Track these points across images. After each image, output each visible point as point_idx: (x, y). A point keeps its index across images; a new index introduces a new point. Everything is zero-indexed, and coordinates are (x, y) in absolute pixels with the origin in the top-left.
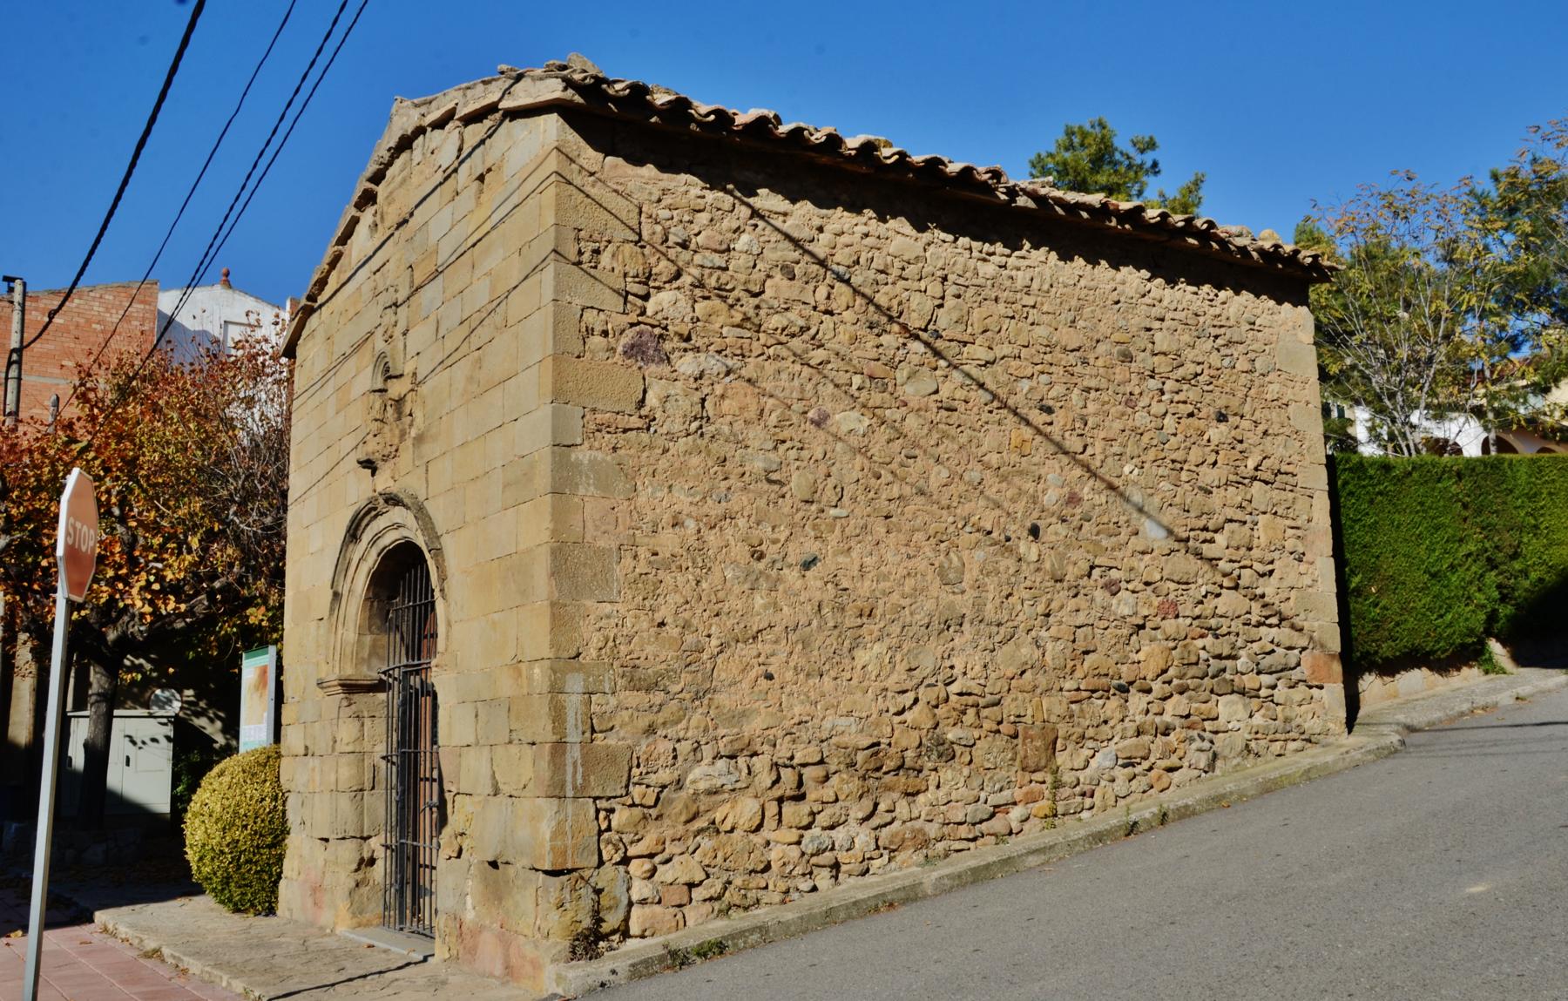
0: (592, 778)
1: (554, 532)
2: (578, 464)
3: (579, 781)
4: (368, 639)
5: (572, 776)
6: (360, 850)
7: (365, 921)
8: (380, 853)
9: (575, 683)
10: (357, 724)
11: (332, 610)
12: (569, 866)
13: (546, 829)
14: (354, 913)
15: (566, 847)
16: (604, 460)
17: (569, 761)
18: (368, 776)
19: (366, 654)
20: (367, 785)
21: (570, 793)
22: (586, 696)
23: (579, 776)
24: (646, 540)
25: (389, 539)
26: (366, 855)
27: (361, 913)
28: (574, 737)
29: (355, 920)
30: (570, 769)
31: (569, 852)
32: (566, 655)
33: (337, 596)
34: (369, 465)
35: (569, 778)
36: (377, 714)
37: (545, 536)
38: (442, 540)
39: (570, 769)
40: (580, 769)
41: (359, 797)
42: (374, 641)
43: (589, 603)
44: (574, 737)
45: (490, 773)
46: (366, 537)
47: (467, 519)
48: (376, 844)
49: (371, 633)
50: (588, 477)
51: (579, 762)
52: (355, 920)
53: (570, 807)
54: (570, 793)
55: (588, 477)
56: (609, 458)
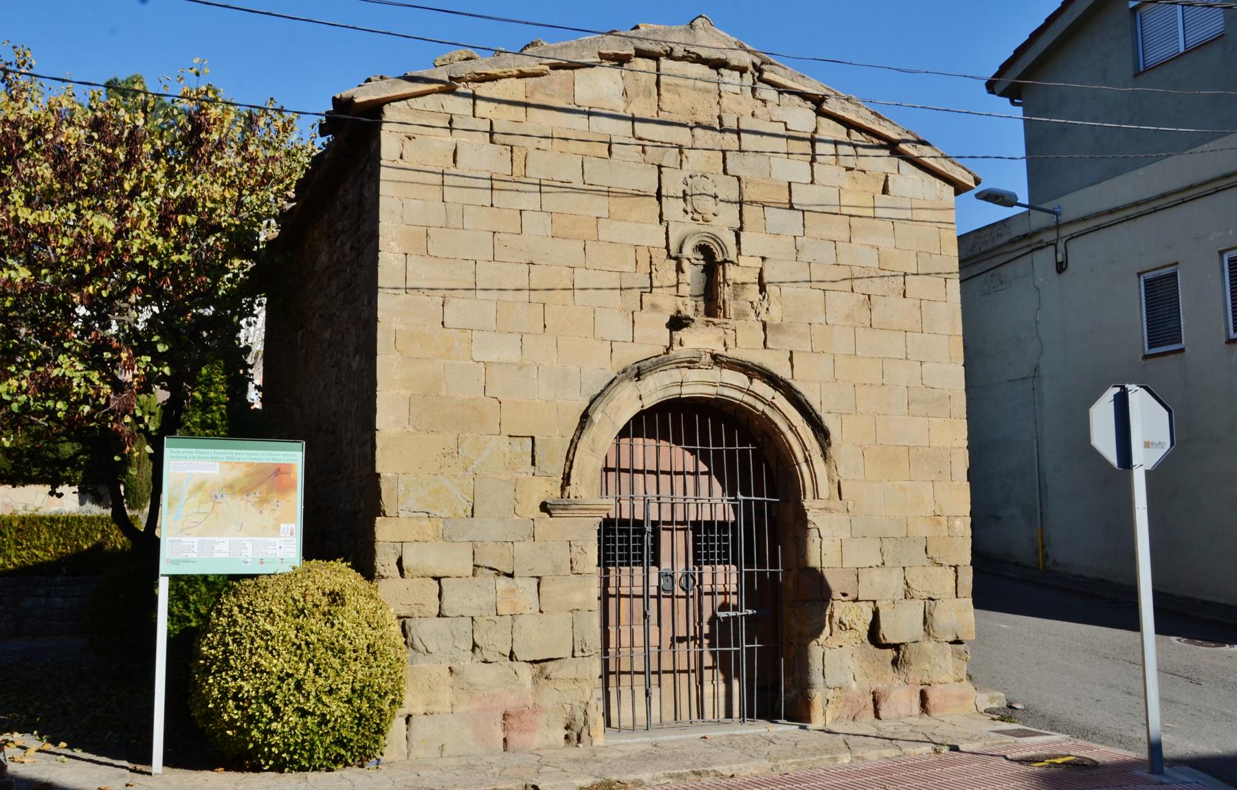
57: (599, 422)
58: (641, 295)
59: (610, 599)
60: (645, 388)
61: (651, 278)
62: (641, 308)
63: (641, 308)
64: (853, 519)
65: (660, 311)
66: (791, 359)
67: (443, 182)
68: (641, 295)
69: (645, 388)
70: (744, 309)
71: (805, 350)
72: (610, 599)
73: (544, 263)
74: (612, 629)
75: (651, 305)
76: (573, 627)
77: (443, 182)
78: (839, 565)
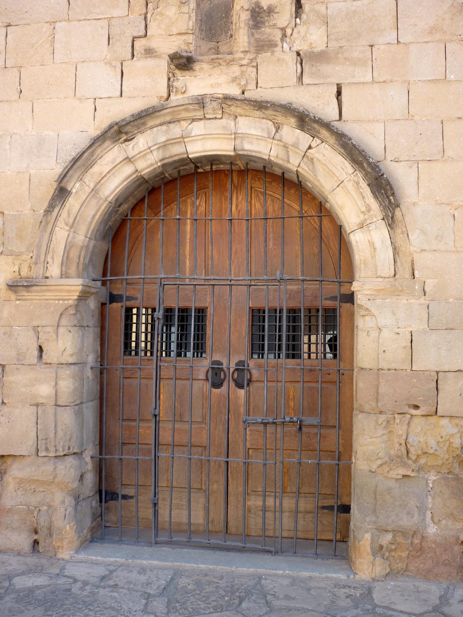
4: (92, 243)
57: (76, 192)
58: (133, 41)
59: (133, 333)
60: (133, 148)
61: (146, 18)
62: (133, 56)
63: (133, 56)
64: (432, 305)
65: (156, 57)
66: (339, 93)
67: (60, 406)
68: (133, 41)
69: (133, 148)
70: (271, 38)
71: (362, 80)
72: (133, 333)
73: (23, 22)
74: (157, 466)
75: (146, 50)
76: (37, 423)
77: (60, 406)
78: (408, 367)
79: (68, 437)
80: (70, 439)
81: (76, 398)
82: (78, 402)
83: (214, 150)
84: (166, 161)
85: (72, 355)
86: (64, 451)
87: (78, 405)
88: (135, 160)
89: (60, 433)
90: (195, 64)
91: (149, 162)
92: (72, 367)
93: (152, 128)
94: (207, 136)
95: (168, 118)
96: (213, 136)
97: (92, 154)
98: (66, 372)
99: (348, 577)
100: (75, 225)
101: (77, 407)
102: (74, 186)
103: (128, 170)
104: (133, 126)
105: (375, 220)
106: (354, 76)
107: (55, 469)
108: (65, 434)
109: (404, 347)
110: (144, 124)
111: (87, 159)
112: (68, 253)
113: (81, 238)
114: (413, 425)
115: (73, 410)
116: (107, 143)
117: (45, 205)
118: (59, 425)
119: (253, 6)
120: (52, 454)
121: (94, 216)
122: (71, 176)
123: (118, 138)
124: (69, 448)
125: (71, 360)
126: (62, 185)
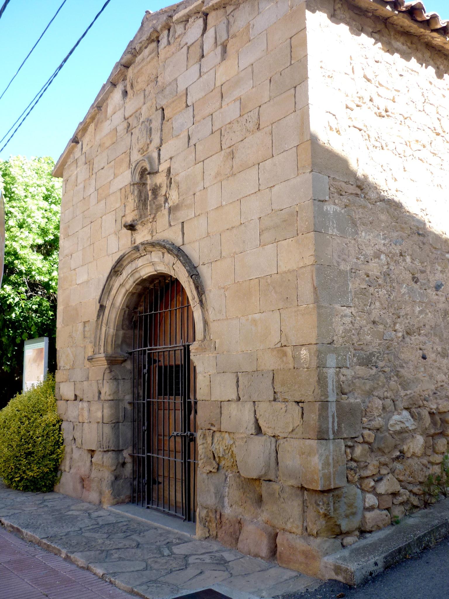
0: (343, 425)
1: (317, 256)
2: (327, 213)
3: (336, 428)
4: (121, 333)
5: (331, 424)
6: (117, 459)
7: (121, 500)
8: (129, 460)
9: (331, 361)
10: (115, 383)
11: (98, 316)
12: (332, 487)
13: (316, 462)
14: (114, 496)
15: (330, 473)
16: (341, 213)
17: (330, 414)
18: (121, 414)
19: (119, 342)
20: (121, 419)
21: (331, 437)
22: (338, 370)
23: (336, 424)
24: (363, 266)
25: (146, 272)
26: (121, 461)
27: (118, 496)
28: (332, 398)
29: (115, 500)
30: (330, 420)
31: (332, 477)
32: (325, 342)
33: (102, 308)
34: (131, 227)
35: (330, 426)
36: (126, 378)
37: (309, 260)
38: (198, 269)
39: (330, 420)
40: (336, 420)
41: (116, 426)
42: (124, 334)
43: (337, 306)
44: (332, 398)
45: (253, 420)
46: (125, 273)
47: (224, 254)
48: (126, 454)
49: (123, 329)
50: (333, 222)
51: (335, 414)
52: (115, 500)
53: (331, 446)
54: (331, 437)
55: (333, 222)
56: (343, 211)
79: (108, 441)
80: (109, 442)
81: (112, 419)
82: (114, 421)
83: (150, 273)
84: (136, 282)
85: (110, 395)
86: (106, 448)
87: (114, 423)
88: (124, 285)
89: (104, 438)
90: (136, 226)
91: (130, 285)
92: (110, 401)
93: (127, 265)
94: (144, 266)
95: (129, 260)
96: (146, 265)
97: (109, 284)
98: (106, 405)
99: (191, 535)
100: (108, 324)
101: (114, 425)
102: (108, 304)
103: (123, 291)
104: (118, 267)
105: (196, 304)
106: (188, 216)
107: (103, 458)
108: (106, 439)
109: (208, 385)
110: (122, 265)
111: (108, 288)
112: (107, 340)
113: (112, 331)
114: (84, 426)
115: (110, 426)
116: (114, 278)
117: (96, 315)
118: (104, 433)
119: (154, 186)
120: (102, 450)
121: (116, 318)
122: (103, 298)
123: (117, 274)
124: (109, 447)
125: (109, 398)
126: (101, 303)
